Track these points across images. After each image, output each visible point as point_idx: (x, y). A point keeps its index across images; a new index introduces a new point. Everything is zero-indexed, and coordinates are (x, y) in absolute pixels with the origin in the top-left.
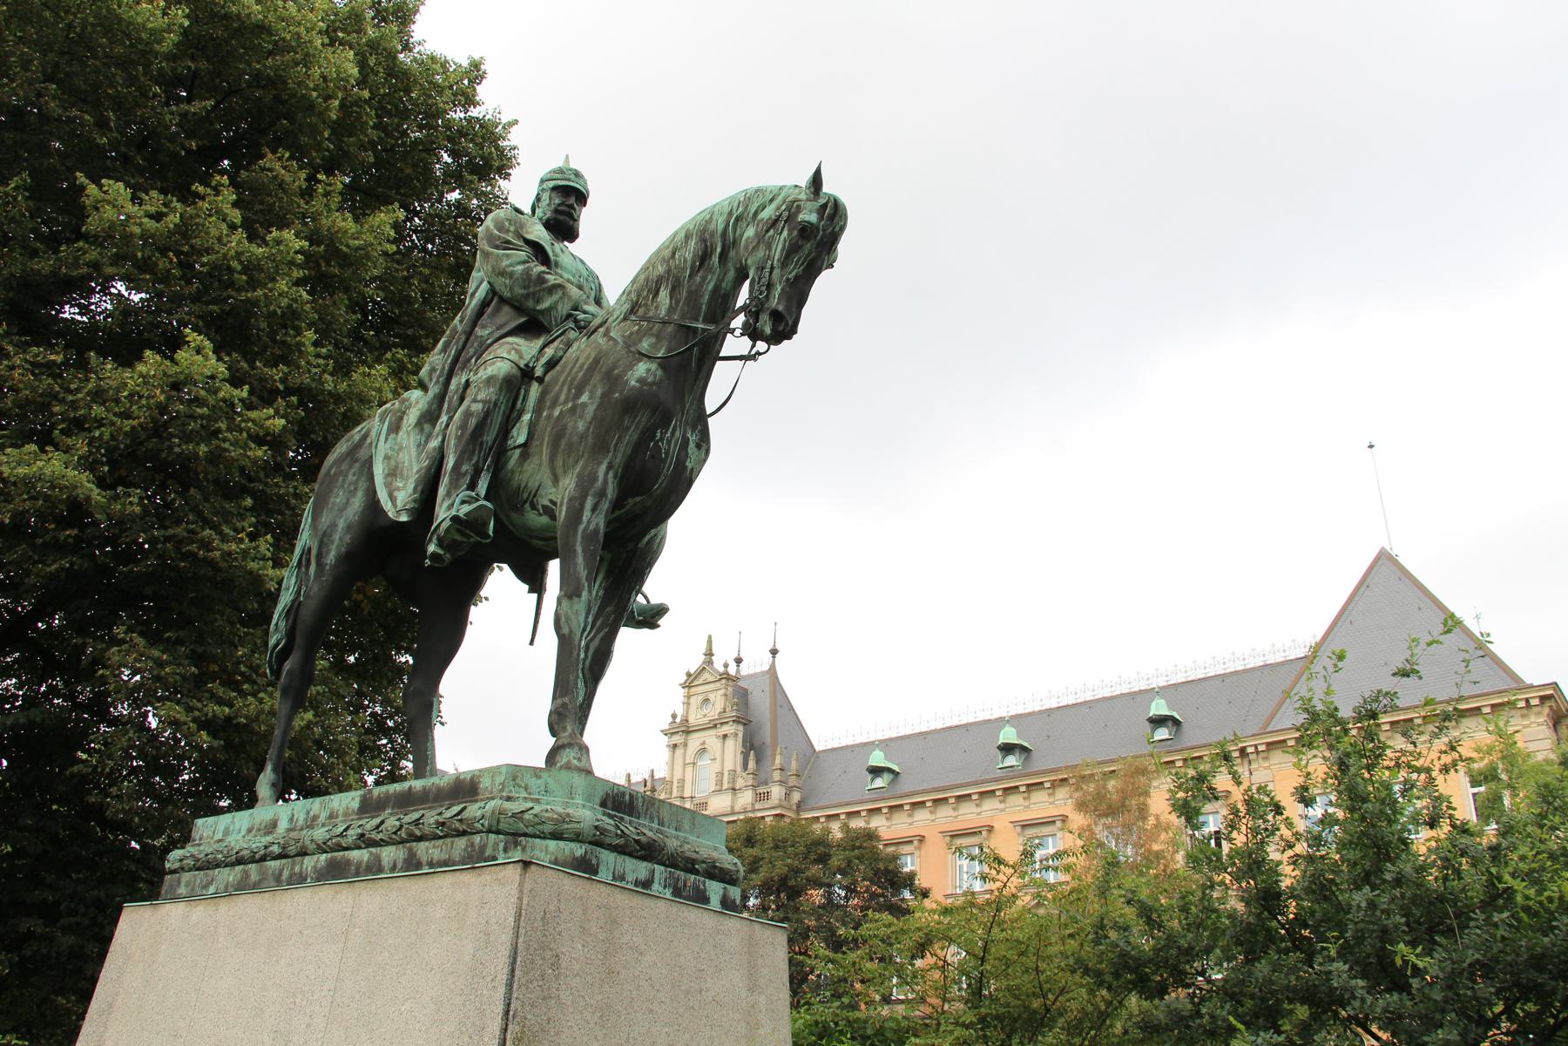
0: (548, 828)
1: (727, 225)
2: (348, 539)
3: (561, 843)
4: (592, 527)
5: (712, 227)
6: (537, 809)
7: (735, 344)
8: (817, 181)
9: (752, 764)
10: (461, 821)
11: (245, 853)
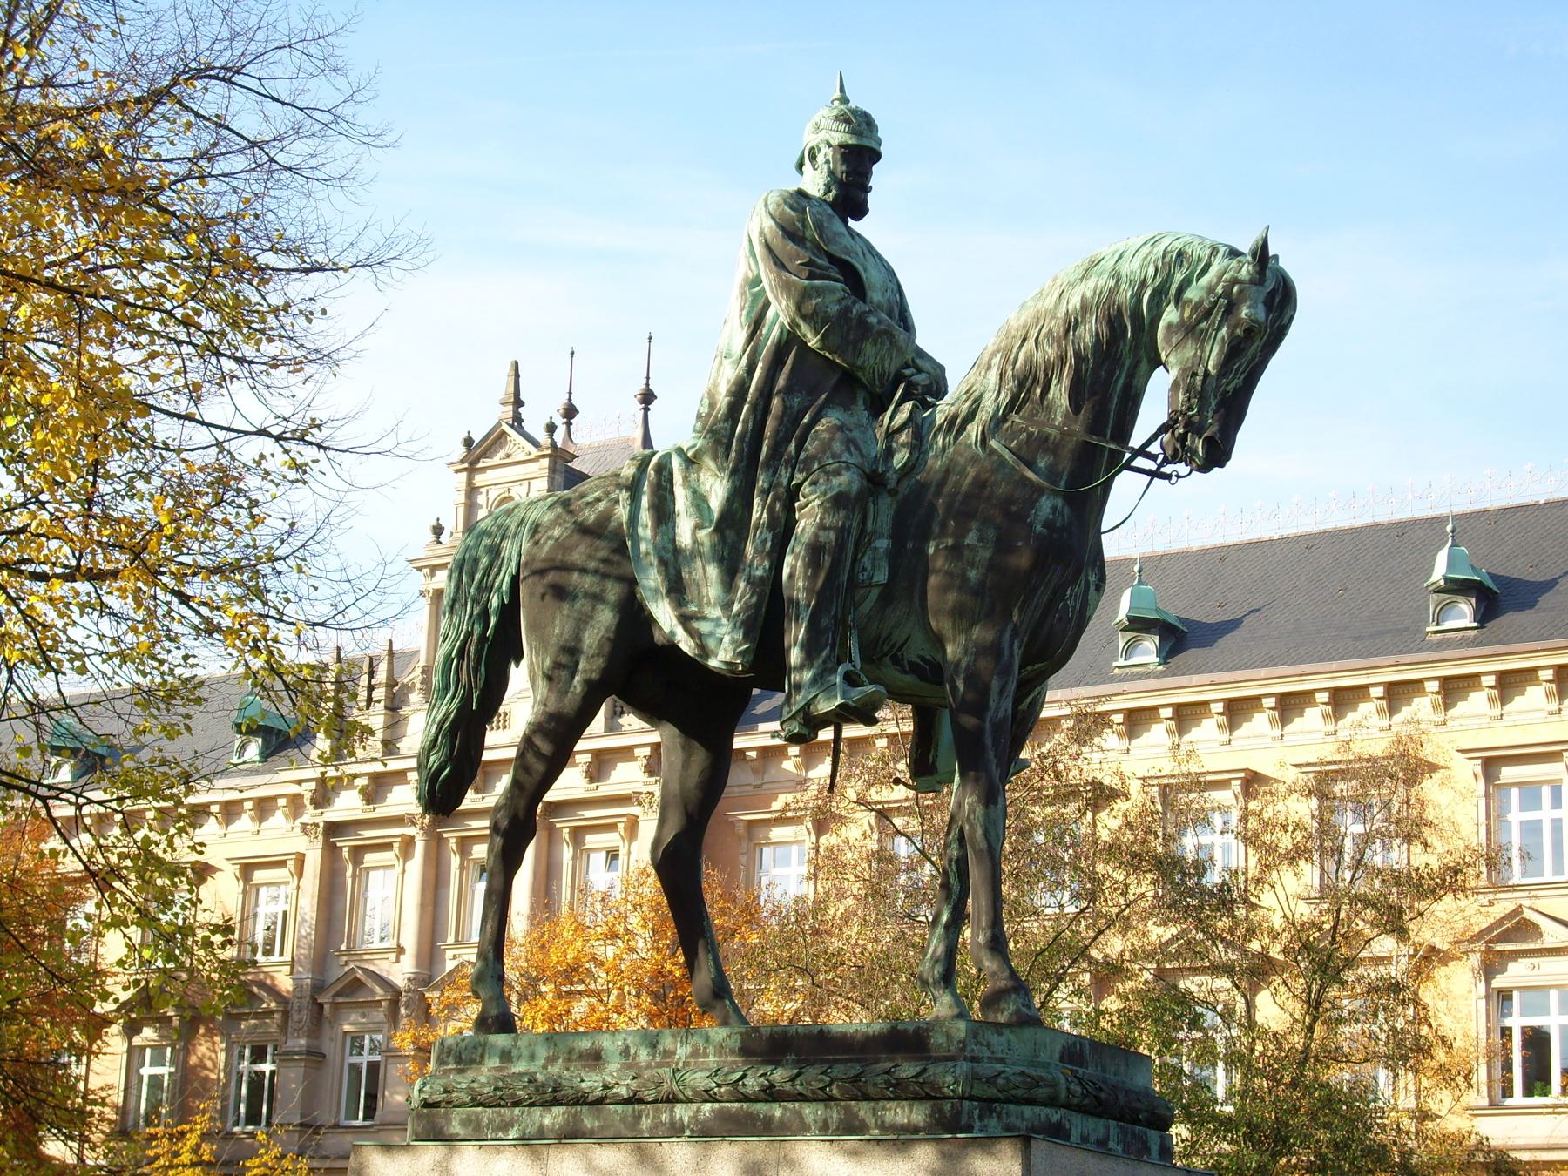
3: (1037, 1109)
4: (1001, 715)
10: (921, 1085)
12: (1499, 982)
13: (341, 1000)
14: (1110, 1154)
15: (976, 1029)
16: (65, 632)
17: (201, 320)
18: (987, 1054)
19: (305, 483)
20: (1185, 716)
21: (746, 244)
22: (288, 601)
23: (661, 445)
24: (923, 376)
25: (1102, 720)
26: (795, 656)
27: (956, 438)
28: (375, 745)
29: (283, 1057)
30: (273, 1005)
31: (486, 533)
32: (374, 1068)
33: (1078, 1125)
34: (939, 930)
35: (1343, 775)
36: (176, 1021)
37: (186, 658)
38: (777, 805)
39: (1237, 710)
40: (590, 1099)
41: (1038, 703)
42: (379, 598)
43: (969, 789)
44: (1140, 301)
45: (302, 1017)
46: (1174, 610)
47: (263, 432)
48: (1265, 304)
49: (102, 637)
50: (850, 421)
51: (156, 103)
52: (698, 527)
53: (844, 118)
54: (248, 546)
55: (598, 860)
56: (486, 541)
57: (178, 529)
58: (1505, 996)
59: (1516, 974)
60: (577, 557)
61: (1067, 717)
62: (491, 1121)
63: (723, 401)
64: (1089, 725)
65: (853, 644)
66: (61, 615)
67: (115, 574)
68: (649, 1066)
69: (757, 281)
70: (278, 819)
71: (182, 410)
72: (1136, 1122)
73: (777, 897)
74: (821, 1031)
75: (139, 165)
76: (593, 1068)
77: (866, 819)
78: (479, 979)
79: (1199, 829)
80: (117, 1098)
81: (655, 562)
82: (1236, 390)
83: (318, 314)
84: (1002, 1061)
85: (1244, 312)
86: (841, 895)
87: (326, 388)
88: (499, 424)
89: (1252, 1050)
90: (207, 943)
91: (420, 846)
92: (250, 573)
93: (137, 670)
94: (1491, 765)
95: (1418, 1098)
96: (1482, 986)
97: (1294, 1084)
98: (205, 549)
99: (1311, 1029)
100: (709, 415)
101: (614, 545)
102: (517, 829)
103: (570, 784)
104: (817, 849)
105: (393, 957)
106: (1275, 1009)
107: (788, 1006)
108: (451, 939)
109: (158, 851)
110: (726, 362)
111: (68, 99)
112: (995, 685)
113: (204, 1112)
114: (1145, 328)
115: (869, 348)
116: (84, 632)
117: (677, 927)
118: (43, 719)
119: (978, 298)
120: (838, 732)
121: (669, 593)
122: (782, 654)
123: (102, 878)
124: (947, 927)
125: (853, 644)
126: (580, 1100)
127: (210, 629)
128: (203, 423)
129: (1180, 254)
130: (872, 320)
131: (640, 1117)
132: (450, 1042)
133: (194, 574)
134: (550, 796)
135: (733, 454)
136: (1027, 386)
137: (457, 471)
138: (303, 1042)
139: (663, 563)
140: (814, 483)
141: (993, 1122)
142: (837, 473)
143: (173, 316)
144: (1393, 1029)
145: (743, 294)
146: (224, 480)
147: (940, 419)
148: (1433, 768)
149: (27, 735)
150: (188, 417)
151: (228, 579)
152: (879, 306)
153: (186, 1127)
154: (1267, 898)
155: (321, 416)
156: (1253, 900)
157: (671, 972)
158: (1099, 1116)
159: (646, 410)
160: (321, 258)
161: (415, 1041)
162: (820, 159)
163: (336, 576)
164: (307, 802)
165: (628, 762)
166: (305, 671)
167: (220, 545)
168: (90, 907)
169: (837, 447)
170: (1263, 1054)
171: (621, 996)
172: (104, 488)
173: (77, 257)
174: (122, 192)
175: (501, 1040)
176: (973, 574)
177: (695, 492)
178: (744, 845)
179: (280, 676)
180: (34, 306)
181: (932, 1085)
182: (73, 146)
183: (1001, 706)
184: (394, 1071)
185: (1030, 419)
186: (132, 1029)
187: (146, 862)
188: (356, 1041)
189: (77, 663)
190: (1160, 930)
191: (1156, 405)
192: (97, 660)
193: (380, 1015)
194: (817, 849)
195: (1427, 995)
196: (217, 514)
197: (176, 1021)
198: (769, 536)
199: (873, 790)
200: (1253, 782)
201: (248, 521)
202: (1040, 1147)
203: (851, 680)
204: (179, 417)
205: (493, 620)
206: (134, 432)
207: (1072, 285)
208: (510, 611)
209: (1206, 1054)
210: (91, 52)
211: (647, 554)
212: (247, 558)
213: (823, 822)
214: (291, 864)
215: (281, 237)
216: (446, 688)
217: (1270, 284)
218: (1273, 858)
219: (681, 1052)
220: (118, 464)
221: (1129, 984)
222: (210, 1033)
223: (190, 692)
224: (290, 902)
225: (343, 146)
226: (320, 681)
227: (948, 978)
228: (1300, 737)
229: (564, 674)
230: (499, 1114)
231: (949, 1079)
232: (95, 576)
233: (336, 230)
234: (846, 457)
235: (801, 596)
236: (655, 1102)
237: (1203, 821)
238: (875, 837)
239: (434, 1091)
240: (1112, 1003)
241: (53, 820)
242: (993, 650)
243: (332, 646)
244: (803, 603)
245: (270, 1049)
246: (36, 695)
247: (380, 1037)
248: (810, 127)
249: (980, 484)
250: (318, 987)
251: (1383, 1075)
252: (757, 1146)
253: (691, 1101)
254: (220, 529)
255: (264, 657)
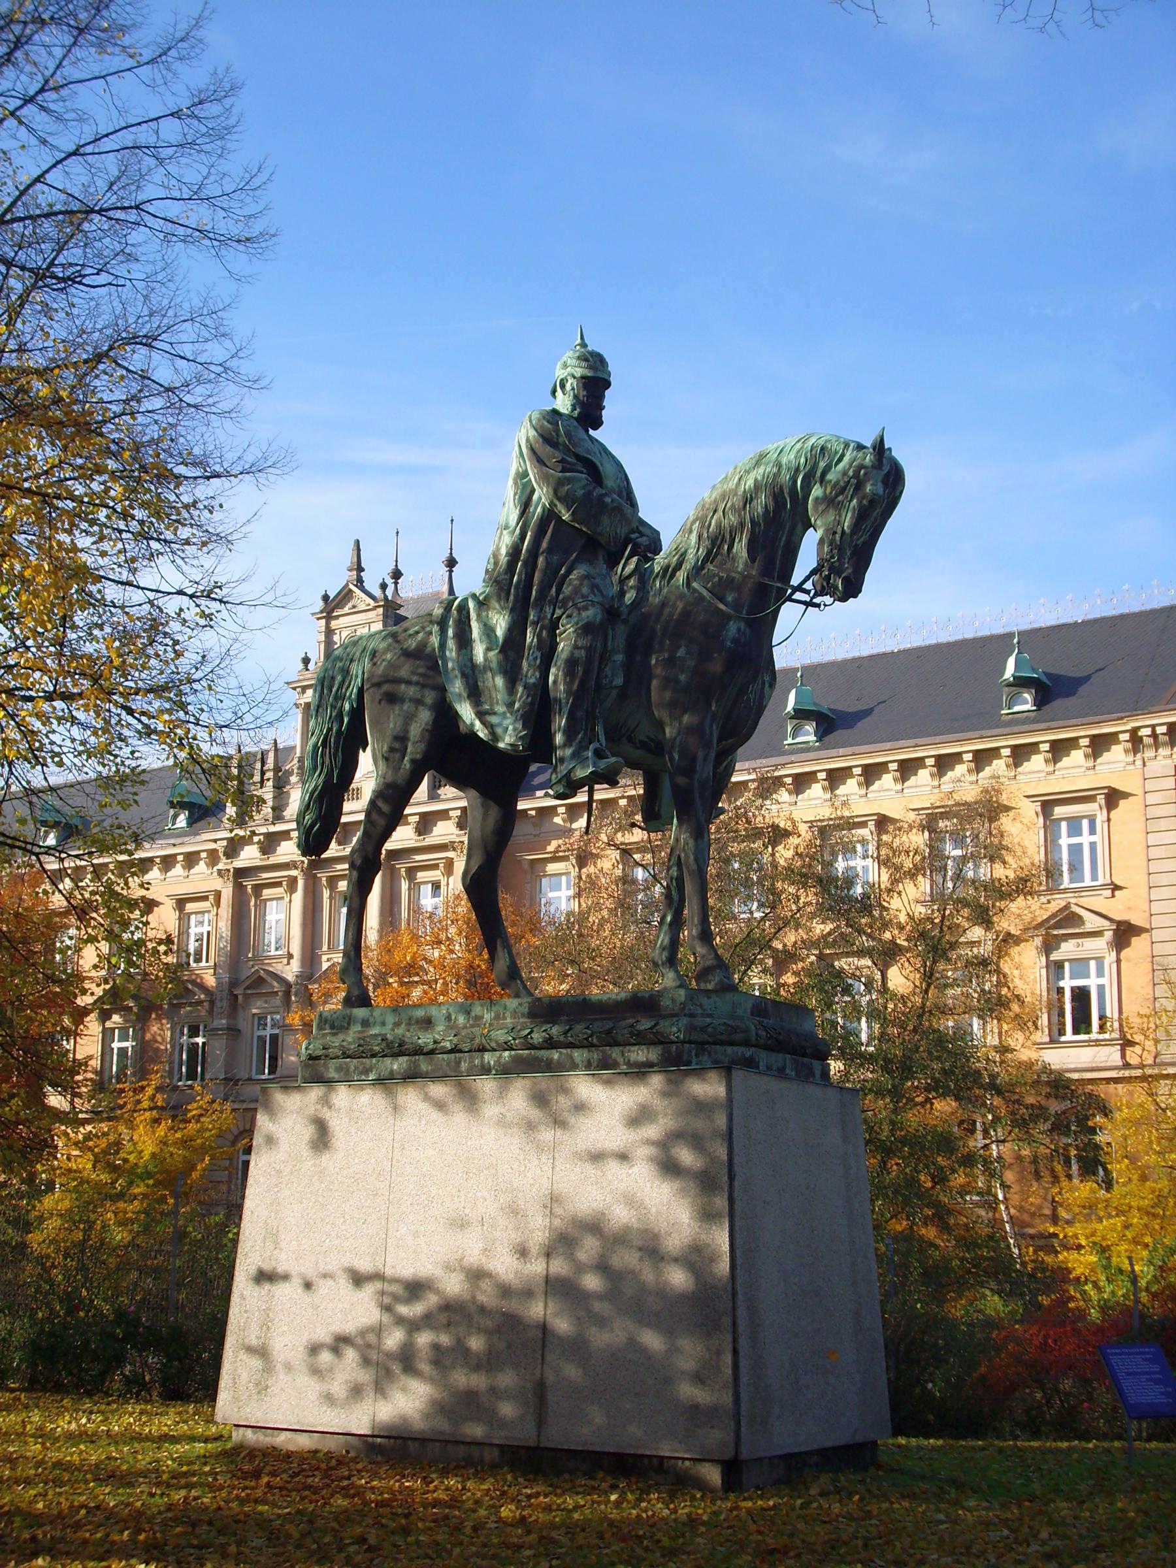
3: (735, 1048)
4: (705, 775)
12: (1054, 956)
13: (249, 992)
14: (787, 1078)
15: (693, 995)
16: (48, 737)
17: (135, 512)
18: (700, 1011)
19: (212, 627)
20: (835, 778)
21: (517, 448)
22: (202, 710)
23: (460, 593)
24: (645, 538)
25: (778, 782)
26: (559, 738)
27: (669, 582)
28: (267, 810)
29: (211, 1033)
30: (202, 996)
31: (339, 658)
32: (274, 1039)
33: (764, 1058)
34: (665, 928)
35: (945, 815)
36: (135, 1010)
37: (133, 753)
38: (550, 848)
39: (871, 773)
40: (425, 1050)
41: (730, 770)
42: (266, 707)
43: (684, 827)
44: (795, 482)
45: (223, 1004)
46: (826, 704)
47: (181, 592)
48: (883, 482)
49: (73, 740)
50: (593, 571)
51: (99, 362)
52: (488, 649)
53: (583, 358)
54: (173, 673)
55: (427, 889)
56: (339, 664)
57: (124, 662)
58: (1059, 965)
59: (1067, 950)
60: (404, 673)
61: (753, 781)
62: (356, 1068)
63: (503, 559)
64: (768, 786)
65: (599, 729)
66: (44, 724)
67: (81, 695)
68: (465, 1027)
69: (525, 474)
70: (201, 867)
71: (124, 578)
72: (804, 1055)
73: (552, 911)
74: (585, 999)
75: (88, 405)
76: (426, 1029)
77: (615, 854)
78: (345, 971)
79: (848, 855)
80: (95, 1063)
81: (459, 676)
82: (864, 543)
83: (217, 508)
84: (710, 1016)
85: (868, 488)
86: (597, 907)
87: (224, 560)
88: (347, 585)
89: (886, 1008)
90: (155, 951)
91: (301, 883)
92: (172, 690)
93: (99, 763)
94: (1047, 806)
95: (1000, 1037)
96: (1044, 959)
97: (915, 1030)
98: (143, 676)
99: (926, 991)
100: (494, 570)
101: (430, 664)
102: (367, 865)
103: (403, 837)
104: (580, 878)
105: (285, 961)
106: (900, 979)
107: (563, 986)
108: (325, 948)
109: (117, 889)
110: (505, 532)
111: (38, 361)
112: (700, 755)
113: (157, 1072)
114: (799, 501)
115: (606, 520)
116: (61, 736)
117: (483, 934)
118: (35, 799)
119: (679, 484)
120: (591, 793)
121: (469, 697)
122: (550, 737)
123: (82, 912)
124: (670, 925)
125: (599, 729)
126: (418, 1051)
127: (148, 732)
128: (138, 587)
129: (823, 448)
130: (608, 500)
131: (460, 1062)
132: (325, 1014)
133: (136, 694)
134: (389, 845)
135: (512, 597)
136: (717, 544)
137: (318, 619)
138: (224, 1021)
139: (464, 675)
140: (569, 616)
141: (706, 1058)
142: (586, 608)
143: (115, 510)
144: (983, 990)
145: (516, 483)
146: (155, 626)
147: (657, 568)
148: (1008, 809)
149: (23, 810)
150: (128, 583)
151: (161, 697)
152: (612, 490)
153: (145, 1083)
154: (895, 903)
155: (222, 580)
156: (885, 904)
157: (479, 966)
158: (779, 1051)
159: (451, 572)
160: (217, 468)
161: (302, 1018)
162: (568, 387)
163: (236, 692)
164: (221, 855)
165: (443, 819)
166: (216, 759)
167: (154, 673)
168: (72, 932)
169: (585, 590)
170: (893, 1010)
171: (445, 984)
172: (72, 635)
173: (46, 473)
174: (76, 424)
175: (360, 1012)
176: (683, 678)
177: (485, 625)
178: (529, 877)
179: (198, 763)
180: (18, 506)
181: (662, 1034)
182: (41, 394)
183: (705, 770)
184: (289, 1040)
185: (720, 567)
186: (105, 1016)
187: (111, 897)
188: (261, 1019)
189: (56, 759)
190: (822, 926)
191: (809, 553)
192: (71, 756)
193: (277, 1001)
194: (580, 878)
195: (1005, 966)
196: (150, 651)
197: (135, 1010)
198: (539, 654)
199: (619, 835)
200: (883, 822)
201: (173, 655)
202: (738, 1075)
203: (599, 754)
204: (122, 583)
205: (346, 720)
206: (90, 594)
207: (748, 472)
208: (358, 713)
209: (855, 1011)
210: (51, 327)
211: (453, 669)
212: (172, 681)
213: (583, 859)
214: (211, 898)
215: (190, 454)
216: (315, 769)
217: (886, 469)
218: (899, 875)
219: (487, 1017)
220: (80, 618)
221: (800, 965)
222: (159, 1018)
223: (137, 777)
224: (210, 926)
225: (230, 389)
226: (227, 766)
227: (672, 961)
228: (914, 790)
229: (397, 756)
230: (362, 1063)
231: (675, 1029)
232: (68, 697)
233: (228, 448)
234: (591, 597)
235: (563, 696)
236: (470, 1051)
237: (849, 850)
238: (620, 866)
239: (316, 1048)
240: (788, 978)
241: (45, 871)
242: (697, 731)
243: (235, 741)
244: (563, 701)
245: (201, 1028)
246: (28, 782)
247: (278, 1017)
248: (559, 365)
249: (686, 614)
250: (234, 983)
251: (976, 1023)
252: (542, 1080)
253: (495, 1050)
254: (153, 662)
255: (187, 750)
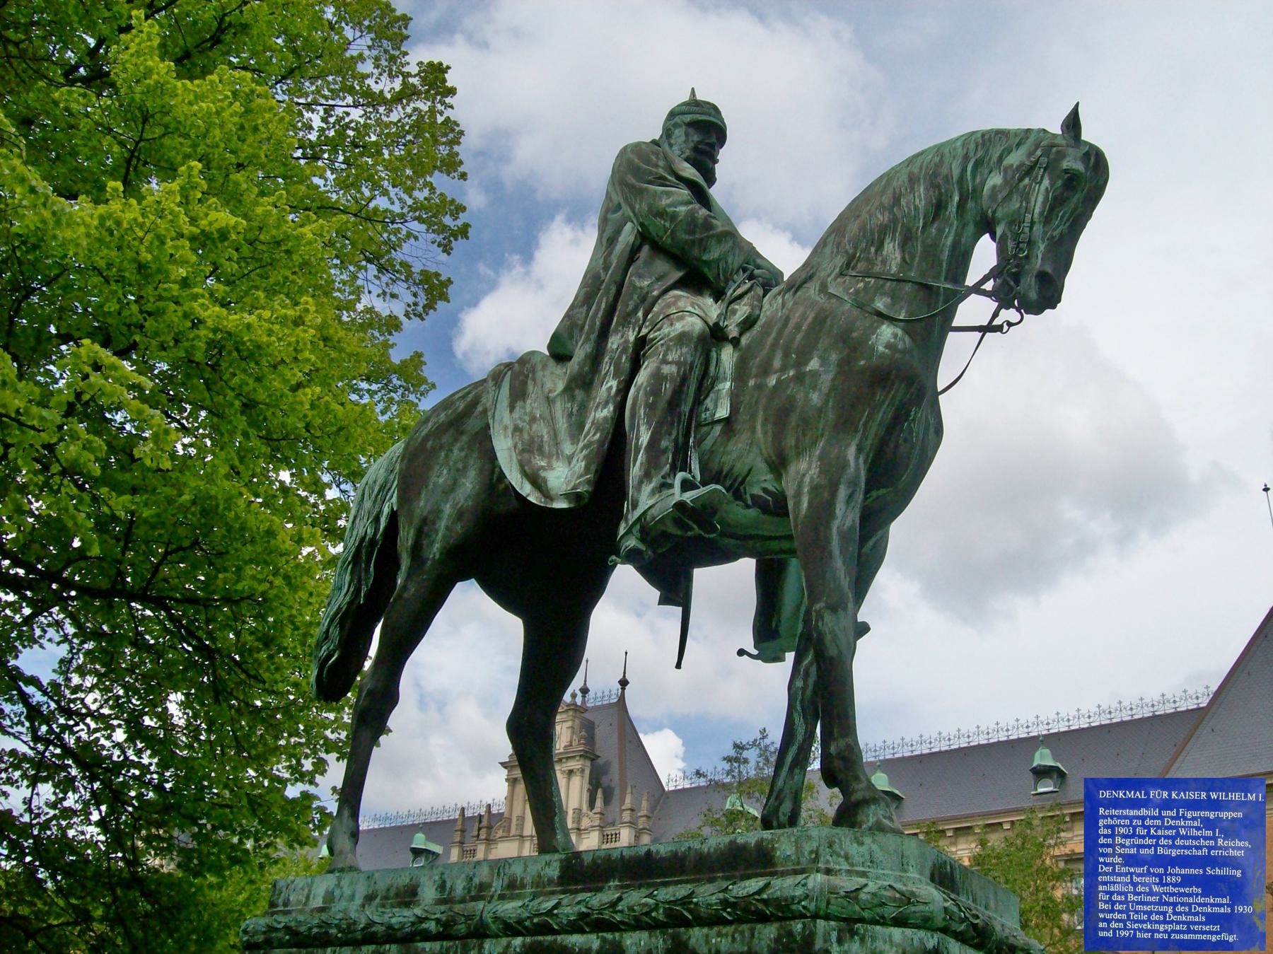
0: (891, 911)
1: (964, 170)
2: (459, 528)
3: (908, 931)
5: (944, 171)
6: (872, 887)
7: (974, 310)
8: (1073, 123)
9: (599, 803)
10: (764, 901)
11: (379, 929)
18: (846, 867)
159: (623, 689)
